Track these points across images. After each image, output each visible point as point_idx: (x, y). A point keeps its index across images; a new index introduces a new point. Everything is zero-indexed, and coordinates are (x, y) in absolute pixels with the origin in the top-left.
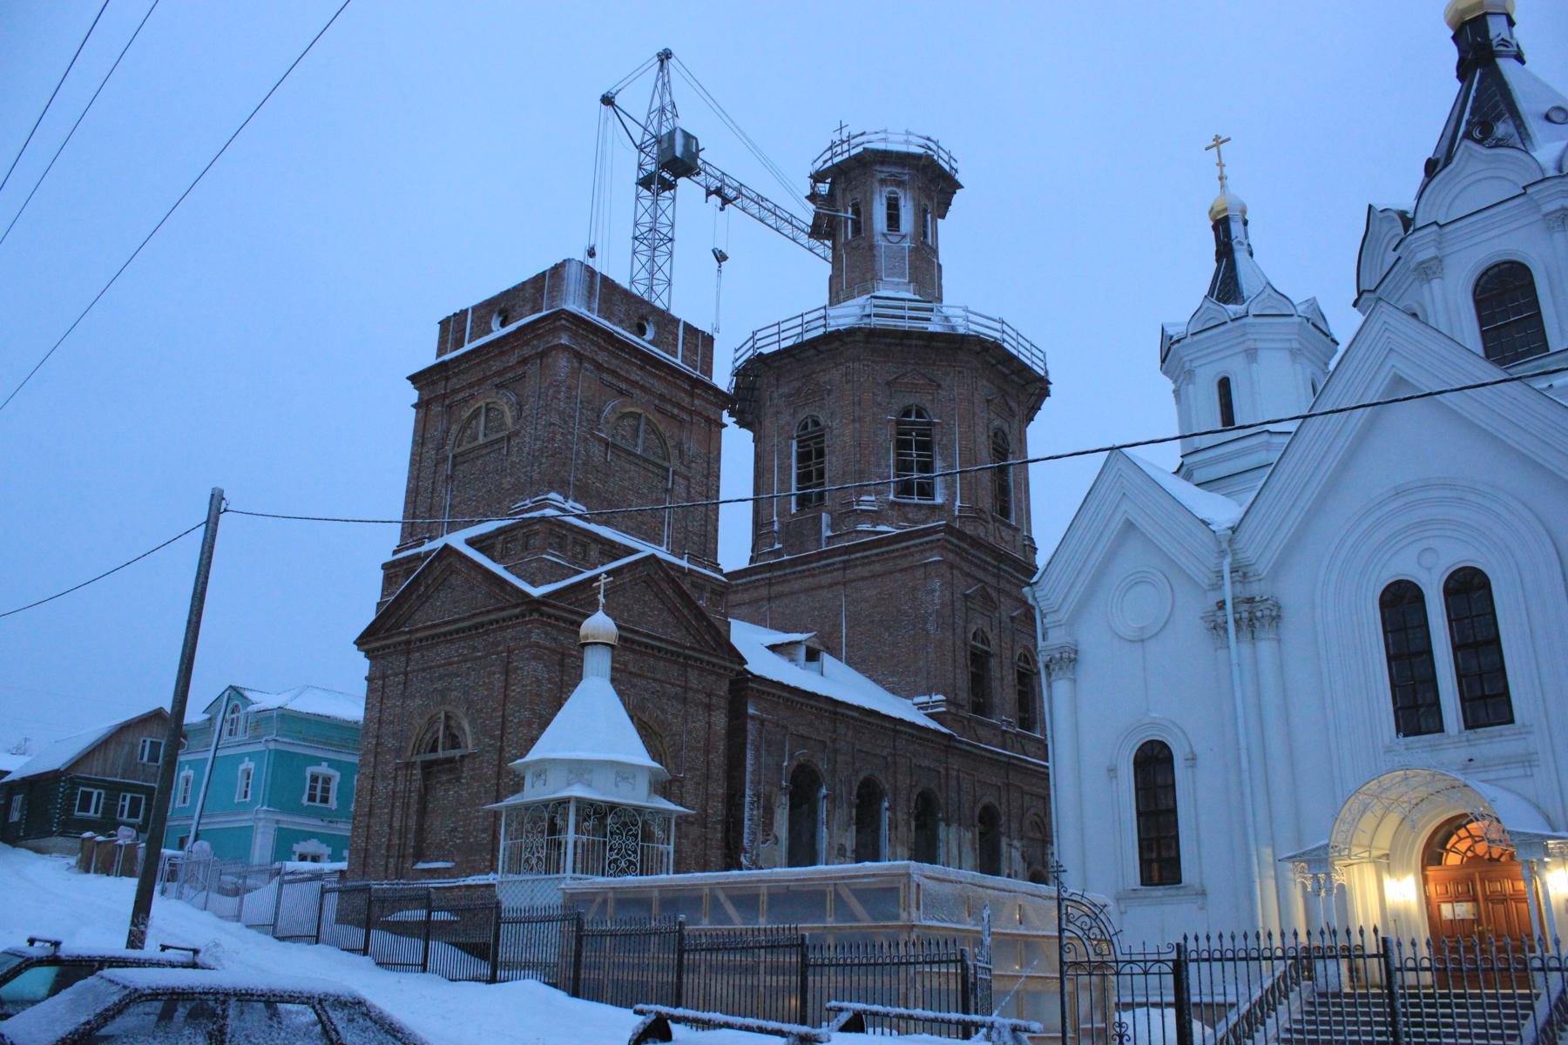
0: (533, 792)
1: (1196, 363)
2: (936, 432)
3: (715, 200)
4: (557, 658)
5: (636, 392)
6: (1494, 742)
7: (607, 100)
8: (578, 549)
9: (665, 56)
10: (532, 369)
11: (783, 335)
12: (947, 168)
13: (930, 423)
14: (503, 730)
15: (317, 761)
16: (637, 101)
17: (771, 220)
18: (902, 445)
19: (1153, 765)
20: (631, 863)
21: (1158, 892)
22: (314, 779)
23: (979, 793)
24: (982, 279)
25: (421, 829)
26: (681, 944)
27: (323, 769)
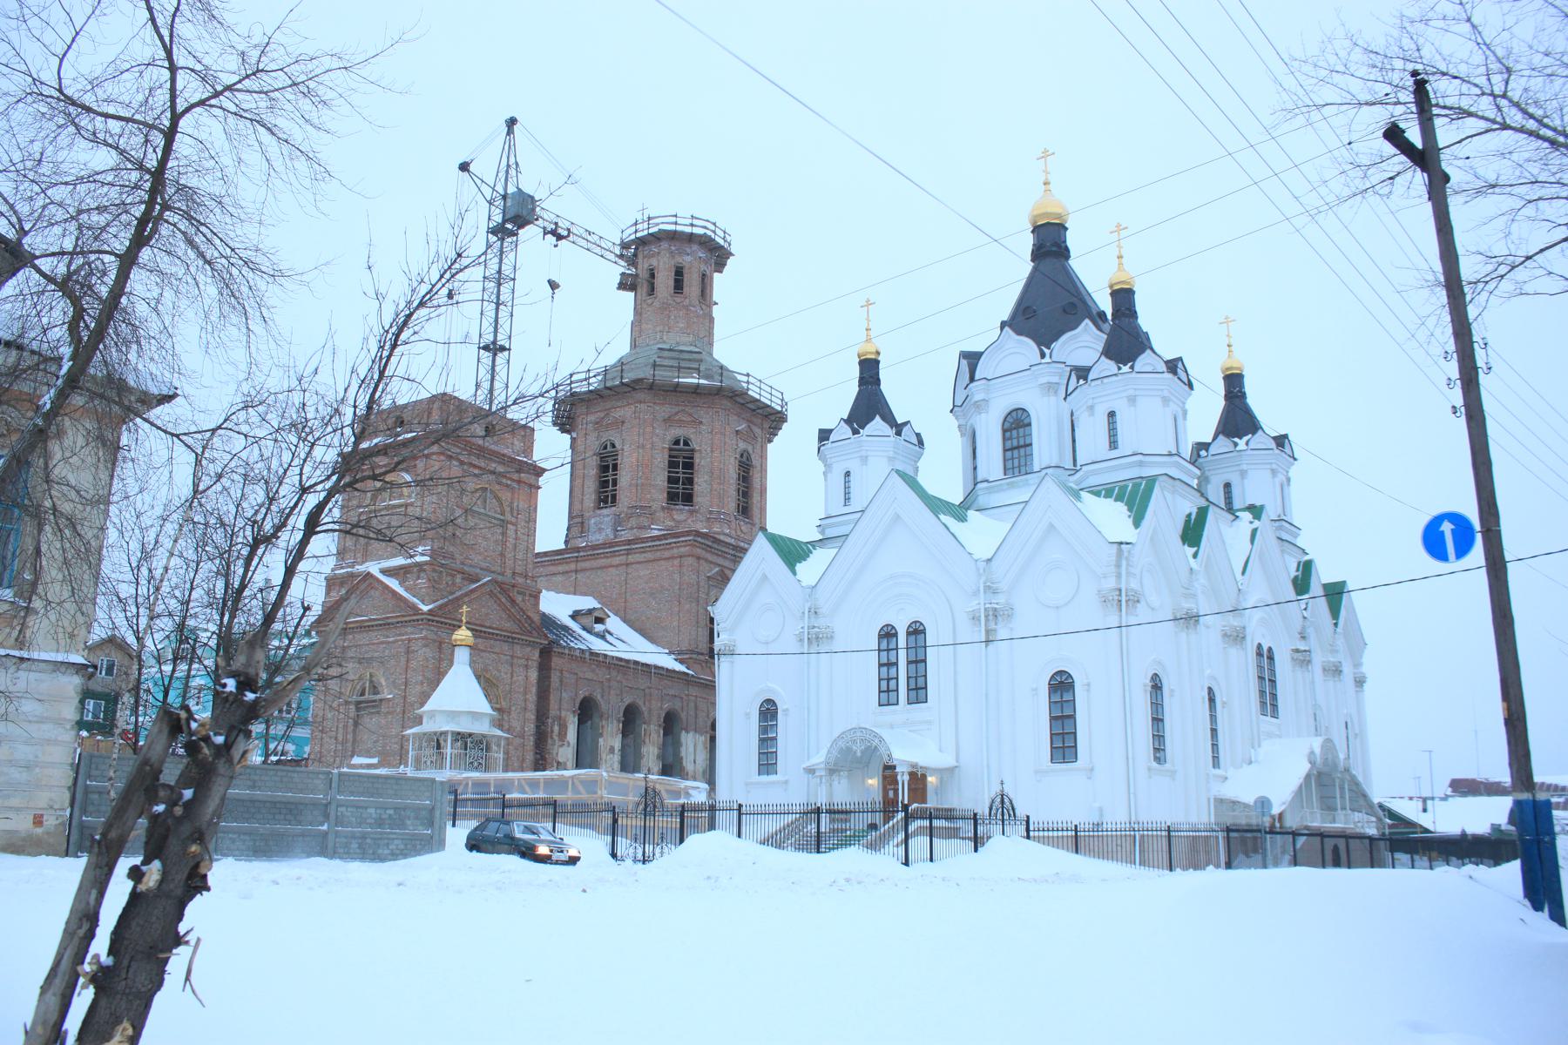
0: (428, 726)
2: (697, 455)
3: (551, 239)
7: (464, 167)
9: (512, 122)
12: (721, 242)
13: (693, 450)
14: (406, 684)
16: (486, 167)
17: (598, 250)
18: (672, 464)
19: (769, 712)
26: (505, 804)
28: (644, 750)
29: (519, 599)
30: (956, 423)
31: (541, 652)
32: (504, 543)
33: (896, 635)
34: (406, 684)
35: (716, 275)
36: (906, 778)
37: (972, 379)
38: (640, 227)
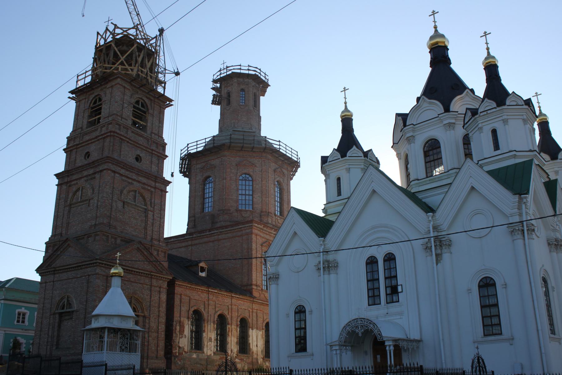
1: (330, 172)
4: (105, 277)
5: (135, 183)
6: (394, 308)
8: (113, 240)
10: (97, 176)
11: (198, 146)
12: (264, 79)
14: (86, 301)
15: (20, 307)
20: (126, 347)
21: (300, 354)
22: (19, 314)
23: (265, 318)
24: (276, 123)
25: (58, 336)
27: (23, 310)
28: (229, 339)
29: (155, 253)
30: (395, 153)
31: (168, 285)
32: (146, 222)
33: (377, 262)
34: (86, 301)
35: (261, 97)
36: (392, 348)
37: (405, 125)
38: (222, 72)
